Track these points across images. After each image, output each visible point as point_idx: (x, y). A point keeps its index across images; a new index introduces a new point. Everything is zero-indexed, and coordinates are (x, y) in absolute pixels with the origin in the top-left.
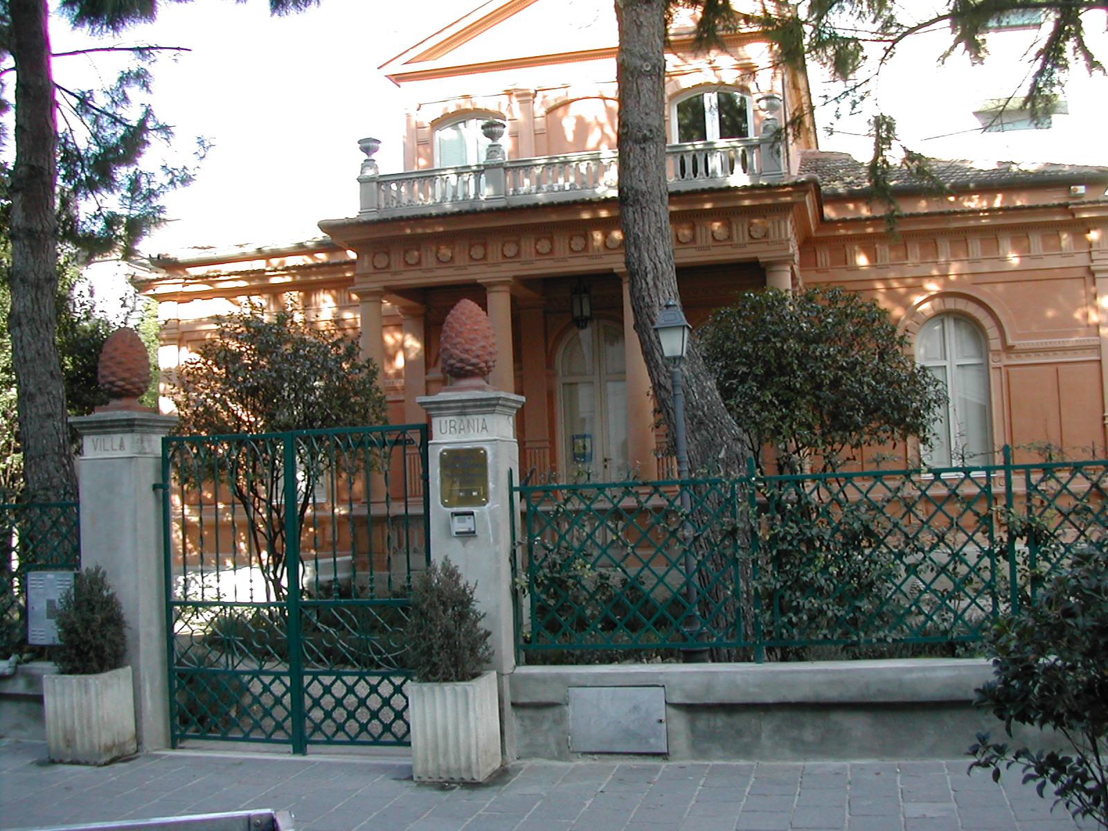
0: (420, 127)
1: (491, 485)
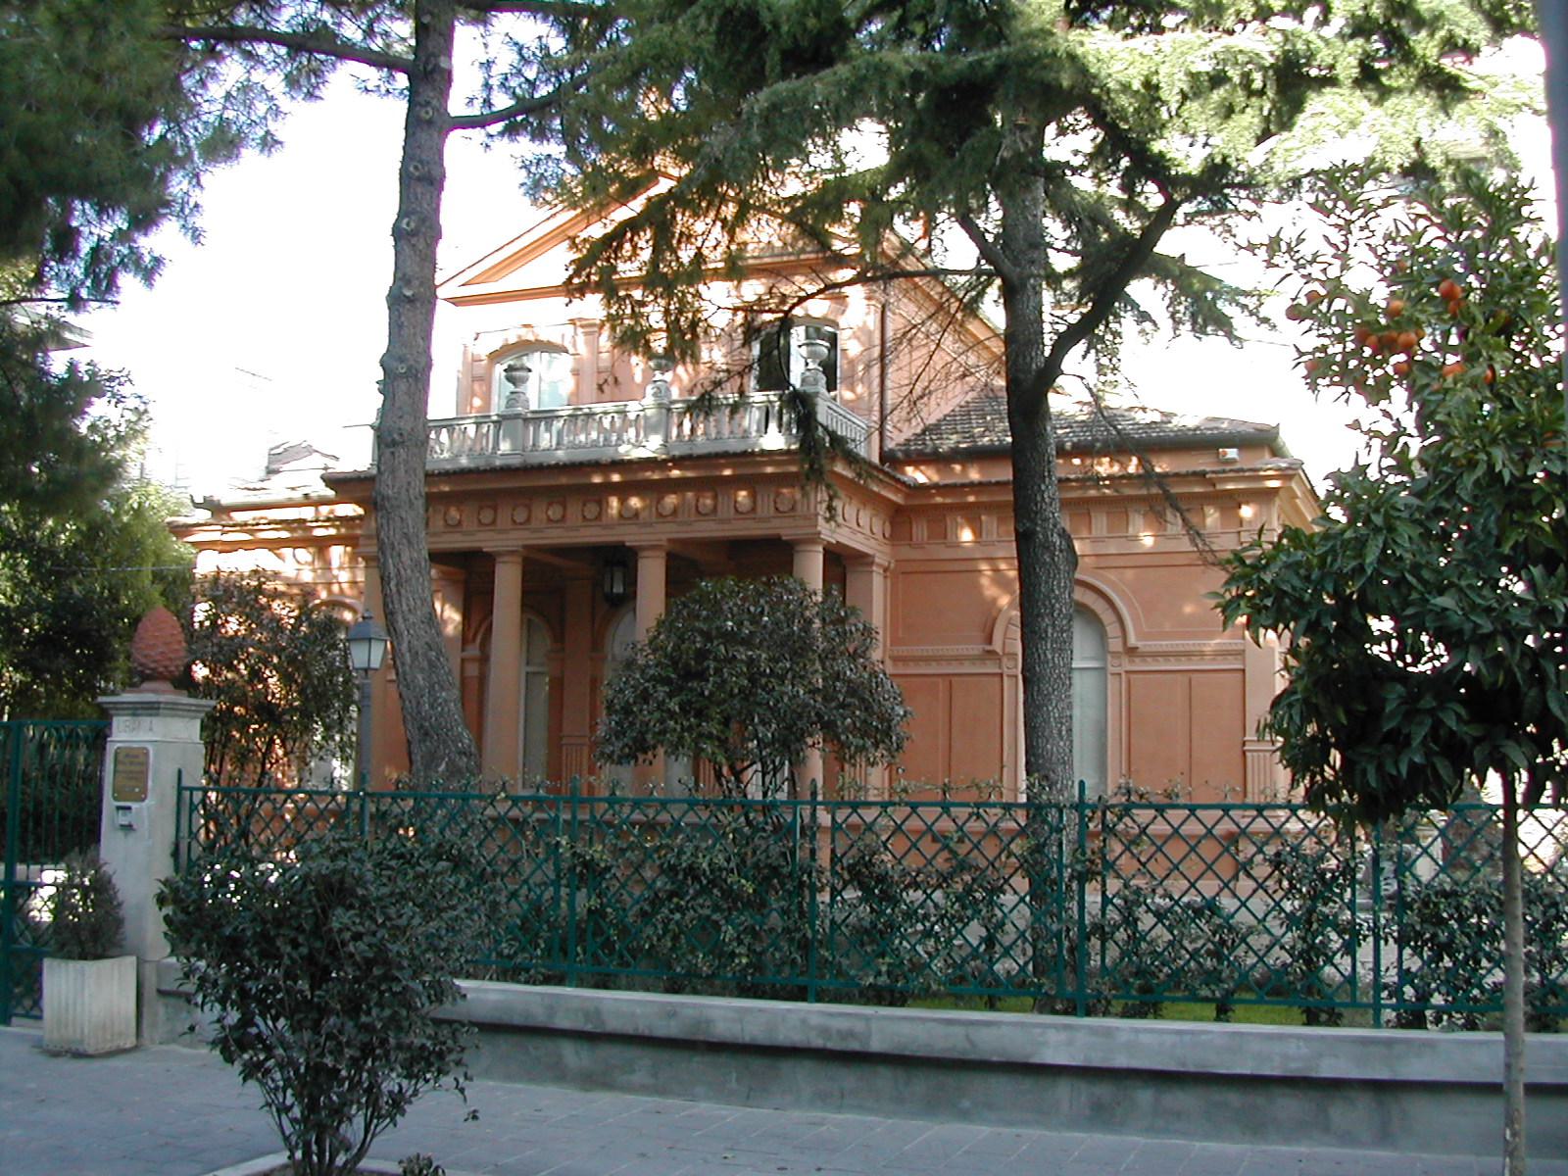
0: (476, 360)
1: (150, 783)
